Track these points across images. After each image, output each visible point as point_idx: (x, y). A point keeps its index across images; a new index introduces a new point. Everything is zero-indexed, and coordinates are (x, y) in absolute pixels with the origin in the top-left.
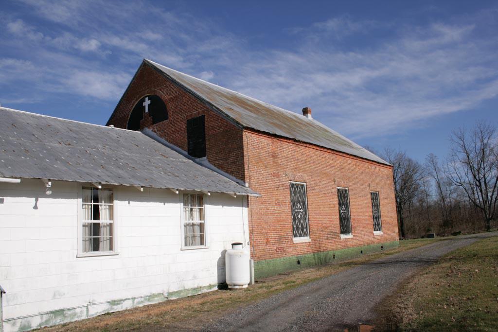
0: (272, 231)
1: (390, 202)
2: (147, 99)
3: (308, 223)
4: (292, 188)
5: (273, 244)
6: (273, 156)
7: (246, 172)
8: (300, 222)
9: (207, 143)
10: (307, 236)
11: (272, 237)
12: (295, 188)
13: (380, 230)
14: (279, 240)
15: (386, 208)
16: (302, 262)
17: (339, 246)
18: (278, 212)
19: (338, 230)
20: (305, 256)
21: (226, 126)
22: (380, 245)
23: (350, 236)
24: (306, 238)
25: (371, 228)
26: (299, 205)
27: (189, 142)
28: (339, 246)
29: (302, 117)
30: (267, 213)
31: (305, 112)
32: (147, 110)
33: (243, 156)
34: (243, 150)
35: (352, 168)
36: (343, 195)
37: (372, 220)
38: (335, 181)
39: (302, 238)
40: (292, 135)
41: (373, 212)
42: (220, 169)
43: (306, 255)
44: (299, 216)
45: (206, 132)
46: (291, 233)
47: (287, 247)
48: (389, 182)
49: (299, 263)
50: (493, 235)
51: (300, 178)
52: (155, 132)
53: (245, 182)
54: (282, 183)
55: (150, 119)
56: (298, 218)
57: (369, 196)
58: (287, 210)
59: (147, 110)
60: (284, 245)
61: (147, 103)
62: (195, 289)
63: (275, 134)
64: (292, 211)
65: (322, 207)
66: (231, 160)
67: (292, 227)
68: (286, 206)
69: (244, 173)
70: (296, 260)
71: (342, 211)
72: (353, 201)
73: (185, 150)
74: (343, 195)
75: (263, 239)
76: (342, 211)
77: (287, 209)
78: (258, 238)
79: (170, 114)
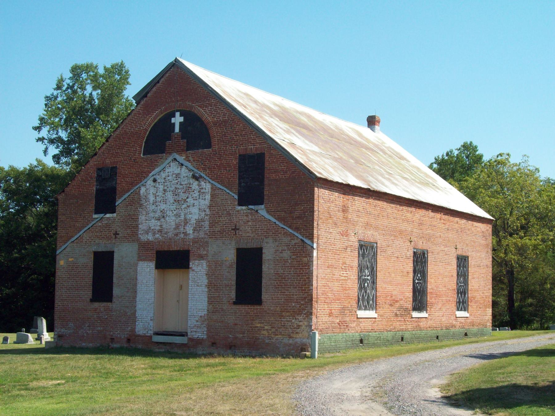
0: (336, 300)
1: (484, 271)
2: (178, 114)
3: (375, 293)
4: (361, 249)
5: (336, 317)
6: (343, 211)
7: (315, 232)
8: (366, 292)
9: (266, 188)
10: (373, 310)
11: (336, 306)
12: (364, 250)
13: (465, 310)
14: (343, 310)
15: (477, 280)
16: (365, 342)
17: (409, 327)
18: (343, 278)
19: (409, 305)
20: (369, 335)
21: (293, 172)
22: (463, 331)
23: (424, 314)
24: (371, 312)
25: (453, 305)
26: (367, 271)
27: (240, 183)
28: (409, 327)
29: (366, 131)
30: (333, 279)
31: (372, 122)
32: (177, 129)
33: (313, 212)
34: (313, 205)
35: (434, 223)
36: (419, 260)
37: (456, 296)
38: (411, 241)
39: (367, 312)
40: (359, 177)
41: (457, 284)
42: (281, 222)
43: (370, 334)
44: (366, 284)
45: (266, 175)
46: (355, 305)
47: (350, 321)
48: (483, 242)
49: (361, 341)
50: (166, 365)
51: (370, 235)
52: (189, 161)
53: (313, 242)
54: (351, 243)
55: (183, 142)
56: (364, 286)
57: (454, 262)
58: (354, 276)
59: (177, 129)
60: (347, 319)
61: (178, 120)
62: (547, 333)
63: (349, 184)
64: (359, 278)
65: (393, 275)
66: (297, 214)
67: (357, 298)
68: (353, 272)
69: (313, 232)
70: (359, 338)
71: (417, 281)
72: (432, 269)
73: (234, 193)
74: (419, 260)
75: (327, 310)
76: (417, 281)
77: (353, 275)
78: (322, 307)
79: (215, 141)
